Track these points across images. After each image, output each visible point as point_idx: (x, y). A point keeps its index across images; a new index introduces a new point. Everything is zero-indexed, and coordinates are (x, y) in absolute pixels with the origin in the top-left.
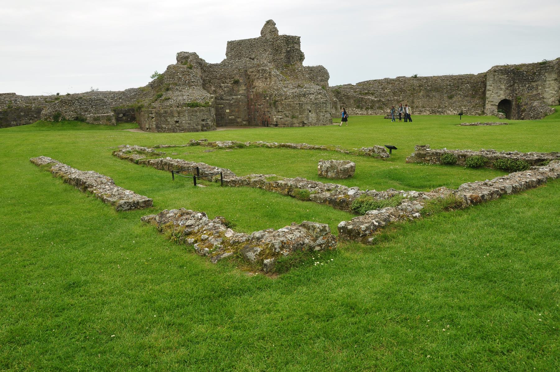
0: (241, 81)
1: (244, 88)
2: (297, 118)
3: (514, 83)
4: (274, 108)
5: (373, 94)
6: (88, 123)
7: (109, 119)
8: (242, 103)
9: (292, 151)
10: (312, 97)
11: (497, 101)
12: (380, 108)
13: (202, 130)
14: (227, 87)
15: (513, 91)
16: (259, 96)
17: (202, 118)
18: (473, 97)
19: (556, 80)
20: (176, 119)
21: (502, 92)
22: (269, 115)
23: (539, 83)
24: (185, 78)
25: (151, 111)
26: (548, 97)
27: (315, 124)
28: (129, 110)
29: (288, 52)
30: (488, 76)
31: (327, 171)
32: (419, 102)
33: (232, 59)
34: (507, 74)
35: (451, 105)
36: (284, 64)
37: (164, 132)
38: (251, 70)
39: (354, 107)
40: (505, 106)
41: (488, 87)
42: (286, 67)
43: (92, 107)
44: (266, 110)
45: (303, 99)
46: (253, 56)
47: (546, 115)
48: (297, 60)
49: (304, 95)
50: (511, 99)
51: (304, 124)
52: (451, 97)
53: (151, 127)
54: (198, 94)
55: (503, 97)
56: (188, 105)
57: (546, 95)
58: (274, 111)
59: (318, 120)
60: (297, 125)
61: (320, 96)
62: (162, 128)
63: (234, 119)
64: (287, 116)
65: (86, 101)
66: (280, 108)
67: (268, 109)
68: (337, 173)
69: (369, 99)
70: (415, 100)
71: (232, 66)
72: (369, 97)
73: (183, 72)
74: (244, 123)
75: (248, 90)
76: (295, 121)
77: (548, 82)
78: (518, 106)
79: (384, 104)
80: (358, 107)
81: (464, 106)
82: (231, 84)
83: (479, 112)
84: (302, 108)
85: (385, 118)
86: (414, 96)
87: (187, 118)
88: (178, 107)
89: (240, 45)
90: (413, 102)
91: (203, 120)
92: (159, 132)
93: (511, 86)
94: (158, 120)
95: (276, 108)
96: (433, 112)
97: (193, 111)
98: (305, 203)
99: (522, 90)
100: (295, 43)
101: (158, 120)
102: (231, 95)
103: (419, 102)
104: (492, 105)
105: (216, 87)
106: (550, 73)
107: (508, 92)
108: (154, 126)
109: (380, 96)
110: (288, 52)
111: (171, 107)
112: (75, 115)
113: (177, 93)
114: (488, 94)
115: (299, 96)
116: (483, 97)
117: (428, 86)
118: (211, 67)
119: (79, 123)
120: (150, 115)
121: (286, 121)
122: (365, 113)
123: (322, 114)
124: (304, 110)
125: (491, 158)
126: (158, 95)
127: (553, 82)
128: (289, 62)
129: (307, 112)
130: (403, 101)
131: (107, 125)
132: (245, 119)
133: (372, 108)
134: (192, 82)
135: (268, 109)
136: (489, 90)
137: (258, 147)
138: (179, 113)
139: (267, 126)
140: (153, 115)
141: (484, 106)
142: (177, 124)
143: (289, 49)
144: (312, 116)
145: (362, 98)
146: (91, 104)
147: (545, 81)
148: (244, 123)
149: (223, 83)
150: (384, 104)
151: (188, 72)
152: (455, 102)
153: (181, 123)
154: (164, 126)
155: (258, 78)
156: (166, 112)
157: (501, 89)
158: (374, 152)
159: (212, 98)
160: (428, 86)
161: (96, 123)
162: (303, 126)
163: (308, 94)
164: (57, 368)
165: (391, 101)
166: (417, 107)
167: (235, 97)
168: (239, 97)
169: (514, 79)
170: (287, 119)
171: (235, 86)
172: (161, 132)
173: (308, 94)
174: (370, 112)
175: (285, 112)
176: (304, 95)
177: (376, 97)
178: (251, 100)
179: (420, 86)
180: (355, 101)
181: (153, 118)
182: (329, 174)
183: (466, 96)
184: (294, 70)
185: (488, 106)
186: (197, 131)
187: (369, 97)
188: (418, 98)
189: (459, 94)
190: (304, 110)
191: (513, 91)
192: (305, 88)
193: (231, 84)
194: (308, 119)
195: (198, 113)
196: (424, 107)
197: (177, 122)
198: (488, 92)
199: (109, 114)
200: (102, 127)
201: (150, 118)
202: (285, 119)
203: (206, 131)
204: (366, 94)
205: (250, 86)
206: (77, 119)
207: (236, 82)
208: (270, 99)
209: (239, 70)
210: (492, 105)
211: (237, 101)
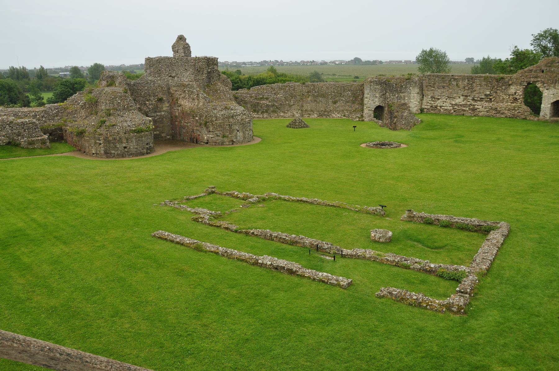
1: (167, 105)
2: (227, 137)
3: (386, 92)
5: (267, 99)
6: (23, 148)
7: (43, 142)
12: (274, 111)
13: (147, 153)
14: (152, 104)
15: (386, 98)
16: (184, 114)
17: (147, 142)
18: (353, 103)
20: (124, 145)
21: (377, 99)
22: (199, 133)
23: (406, 94)
25: (99, 138)
26: (413, 106)
27: (242, 142)
28: (56, 129)
29: (209, 73)
30: (365, 86)
31: (379, 238)
32: (307, 106)
33: (151, 75)
38: (175, 89)
40: (379, 111)
41: (366, 95)
43: (25, 131)
44: (195, 128)
45: (231, 120)
46: (174, 75)
47: (415, 125)
49: (232, 117)
50: (384, 105)
52: (335, 103)
53: (98, 152)
55: (377, 104)
56: (134, 131)
58: (204, 130)
59: (244, 138)
60: (228, 143)
61: (244, 116)
62: (111, 153)
63: (159, 135)
65: (18, 125)
67: (198, 128)
68: (386, 239)
70: (304, 105)
71: (154, 84)
74: (168, 137)
76: (226, 140)
77: (412, 95)
78: (391, 113)
79: (277, 108)
80: (254, 111)
81: (346, 110)
84: (231, 128)
86: (303, 101)
87: (135, 144)
89: (159, 62)
90: (303, 106)
91: (147, 144)
92: (107, 157)
93: (383, 95)
94: (106, 146)
95: (207, 128)
96: (320, 115)
97: (139, 137)
98: (408, 271)
99: (393, 99)
100: (215, 64)
102: (156, 112)
103: (307, 106)
105: (141, 104)
107: (381, 99)
108: (102, 152)
110: (209, 73)
112: (7, 140)
114: (366, 101)
115: (228, 117)
116: (362, 104)
117: (315, 92)
118: (134, 85)
119: (14, 148)
120: (98, 141)
121: (217, 140)
123: (247, 132)
124: (234, 130)
125: (454, 222)
126: (101, 121)
127: (416, 95)
128: (210, 82)
129: (236, 131)
131: (41, 148)
134: (131, 106)
135: (198, 128)
136: (366, 98)
139: (197, 143)
140: (101, 142)
141: (362, 110)
142: (126, 150)
143: (209, 70)
144: (240, 134)
145: (258, 103)
146: (23, 128)
147: (410, 93)
148: (168, 137)
150: (277, 108)
152: (338, 107)
153: (130, 148)
154: (113, 152)
155: (183, 98)
156: (115, 139)
157: (376, 97)
158: (377, 211)
160: (315, 92)
161: (31, 148)
162: (233, 144)
163: (235, 116)
164: (81, 369)
165: (284, 105)
166: (306, 110)
167: (159, 114)
168: (163, 113)
169: (386, 89)
170: (218, 138)
172: (110, 158)
173: (235, 116)
174: (265, 116)
175: (217, 132)
176: (232, 117)
178: (176, 117)
179: (308, 92)
180: (252, 105)
181: (100, 144)
182: (381, 240)
184: (216, 91)
189: (342, 100)
190: (234, 130)
191: (386, 98)
192: (232, 110)
194: (236, 138)
195: (143, 138)
196: (312, 111)
197: (125, 147)
199: (43, 137)
200: (38, 151)
202: (216, 138)
203: (150, 153)
204: (261, 98)
205: (175, 104)
206: (9, 143)
207: (160, 100)
208: (200, 119)
209: (162, 88)
211: (162, 117)
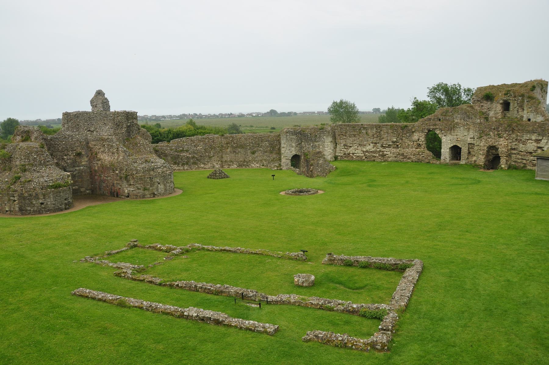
0: (83, 153)
2: (148, 190)
3: (302, 142)
4: (125, 182)
5: (187, 151)
8: (85, 173)
9: (232, 256)
10: (160, 170)
11: (290, 156)
12: (194, 163)
13: (66, 209)
14: (70, 159)
15: (301, 148)
16: (104, 168)
17: (65, 198)
18: (271, 152)
19: (331, 142)
20: (41, 201)
21: (293, 149)
22: (119, 187)
23: (320, 143)
24: (40, 157)
26: (327, 154)
27: (164, 194)
31: (303, 283)
33: (69, 130)
34: (296, 134)
35: (254, 160)
36: (125, 138)
37: (29, 214)
38: (93, 143)
39: (171, 164)
40: (295, 160)
41: (282, 145)
42: (128, 140)
44: (116, 182)
45: (152, 173)
46: (92, 129)
48: (136, 134)
49: (153, 170)
50: (300, 154)
51: (154, 195)
52: (253, 153)
53: (12, 209)
54: (52, 174)
55: (294, 153)
57: (325, 153)
58: (125, 184)
59: (166, 190)
60: (149, 196)
61: (165, 169)
62: (26, 210)
64: (138, 189)
66: (132, 182)
67: (118, 182)
69: (184, 156)
70: (224, 156)
71: (72, 139)
72: (184, 154)
73: (37, 152)
75: (90, 161)
76: (147, 192)
77: (326, 143)
78: (307, 161)
79: (198, 160)
80: (175, 163)
82: (74, 156)
83: (277, 164)
84: (152, 181)
85: (208, 177)
87: (52, 199)
88: (42, 189)
90: (222, 157)
91: (66, 199)
92: (23, 214)
93: (299, 144)
94: (21, 202)
95: (128, 181)
96: (240, 166)
97: (57, 193)
99: (308, 147)
100: (134, 118)
101: (21, 202)
102: (74, 166)
104: (287, 159)
105: (59, 159)
106: (327, 136)
107: (297, 148)
108: (17, 209)
109: (194, 153)
111: (35, 190)
113: (36, 175)
114: (283, 150)
115: (149, 170)
116: (279, 153)
120: (12, 198)
122: (182, 168)
123: (168, 185)
124: (154, 182)
126: (16, 177)
128: (129, 136)
129: (156, 184)
130: (213, 156)
132: (88, 188)
133: (187, 164)
134: (48, 161)
135: (118, 182)
137: (200, 250)
138: (44, 195)
141: (280, 160)
142: (43, 206)
143: (129, 124)
144: (161, 187)
145: (178, 155)
147: (324, 142)
149: (66, 156)
150: (198, 160)
151: (42, 151)
152: (257, 157)
153: (47, 204)
154: (29, 208)
155: (102, 152)
156: (30, 195)
157: (292, 146)
159: (68, 176)
163: (156, 168)
165: (204, 156)
166: (226, 161)
167: (77, 168)
168: (82, 168)
171: (77, 158)
174: (186, 167)
175: (137, 185)
176: (153, 170)
177: (190, 154)
178: (95, 171)
179: (227, 144)
180: (172, 158)
181: (15, 201)
183: (266, 152)
185: (283, 160)
186: (61, 210)
187: (184, 154)
188: (226, 154)
190: (154, 182)
191: (301, 148)
192: (152, 162)
193: (74, 156)
194: (157, 190)
195: (62, 194)
196: (231, 162)
197: (42, 204)
198: (283, 149)
201: (12, 201)
202: (137, 191)
203: (68, 209)
204: (181, 151)
205: (94, 158)
207: (79, 155)
208: (120, 172)
210: (287, 159)
211: (80, 172)
